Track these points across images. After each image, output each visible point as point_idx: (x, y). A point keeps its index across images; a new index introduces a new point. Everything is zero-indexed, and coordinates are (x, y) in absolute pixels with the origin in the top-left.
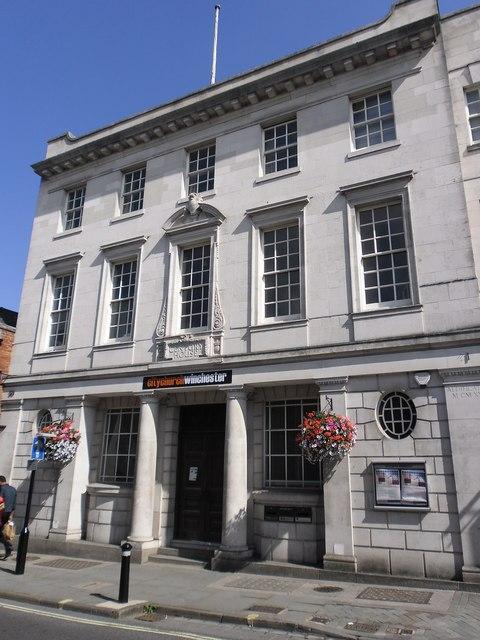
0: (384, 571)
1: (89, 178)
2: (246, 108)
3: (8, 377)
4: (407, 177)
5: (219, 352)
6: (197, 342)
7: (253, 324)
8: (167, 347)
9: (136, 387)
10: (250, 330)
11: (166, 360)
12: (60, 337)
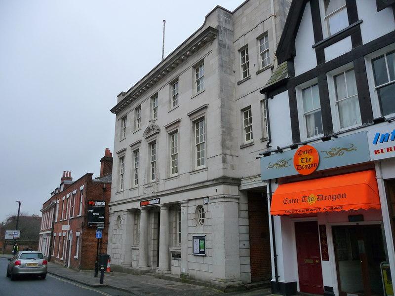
9: (137, 205)
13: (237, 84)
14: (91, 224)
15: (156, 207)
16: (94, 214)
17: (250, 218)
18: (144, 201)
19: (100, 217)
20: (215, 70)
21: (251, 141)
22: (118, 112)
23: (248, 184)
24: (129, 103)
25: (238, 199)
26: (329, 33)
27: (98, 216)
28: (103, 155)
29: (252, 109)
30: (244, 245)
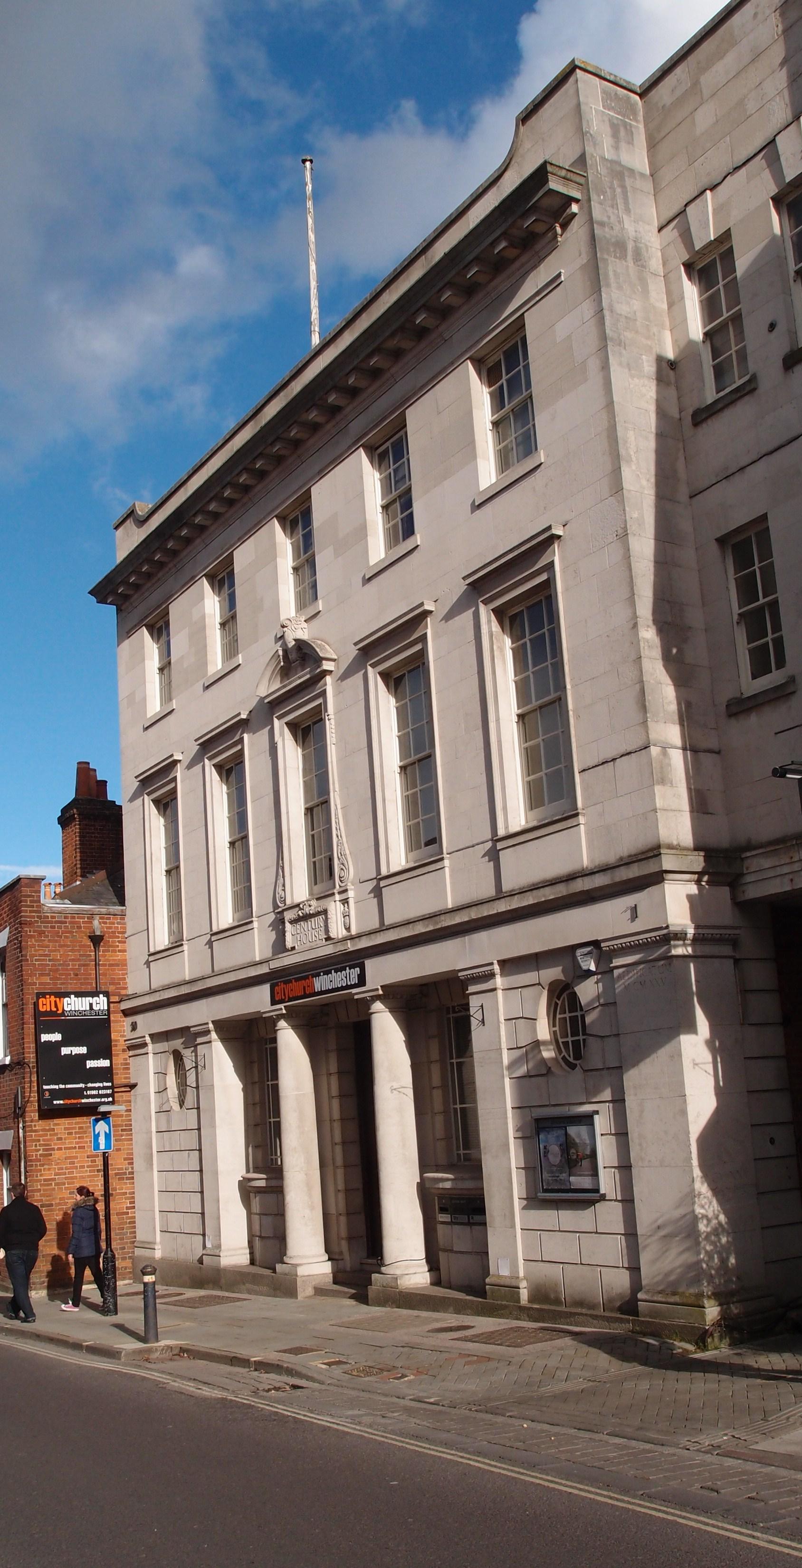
0: (557, 1301)
1: (310, 488)
2: (338, 417)
3: (130, 997)
4: (546, 541)
5: (348, 929)
6: (318, 914)
7: (501, 832)
8: (288, 925)
9: (258, 1000)
10: (380, 884)
11: (288, 950)
12: (426, 837)
13: (688, 420)
14: (55, 1094)
15: (350, 1001)
16: (65, 1051)
17: (787, 1021)
18: (285, 981)
19: (90, 1064)
20: (584, 363)
21: (773, 679)
22: (126, 597)
23: (779, 871)
24: (174, 553)
25: (734, 943)
26: (507, 827)
27: (83, 1058)
28: (68, 794)
29: (771, 523)
30: (772, 1141)
